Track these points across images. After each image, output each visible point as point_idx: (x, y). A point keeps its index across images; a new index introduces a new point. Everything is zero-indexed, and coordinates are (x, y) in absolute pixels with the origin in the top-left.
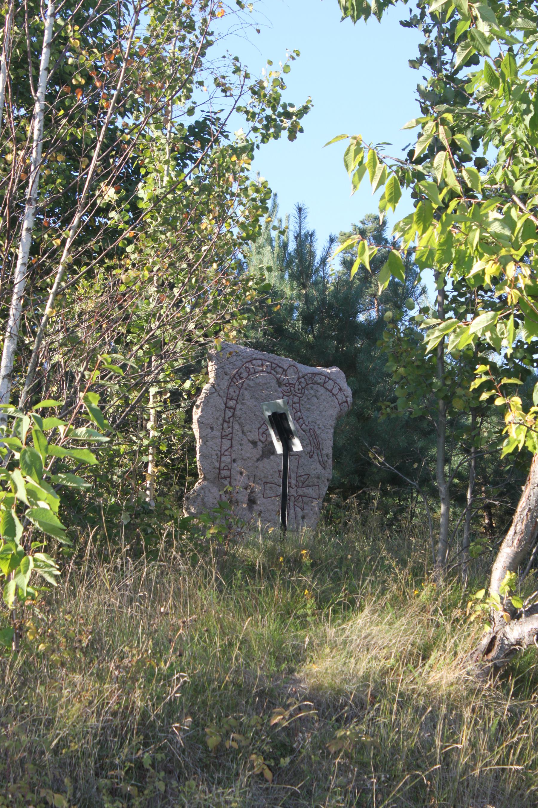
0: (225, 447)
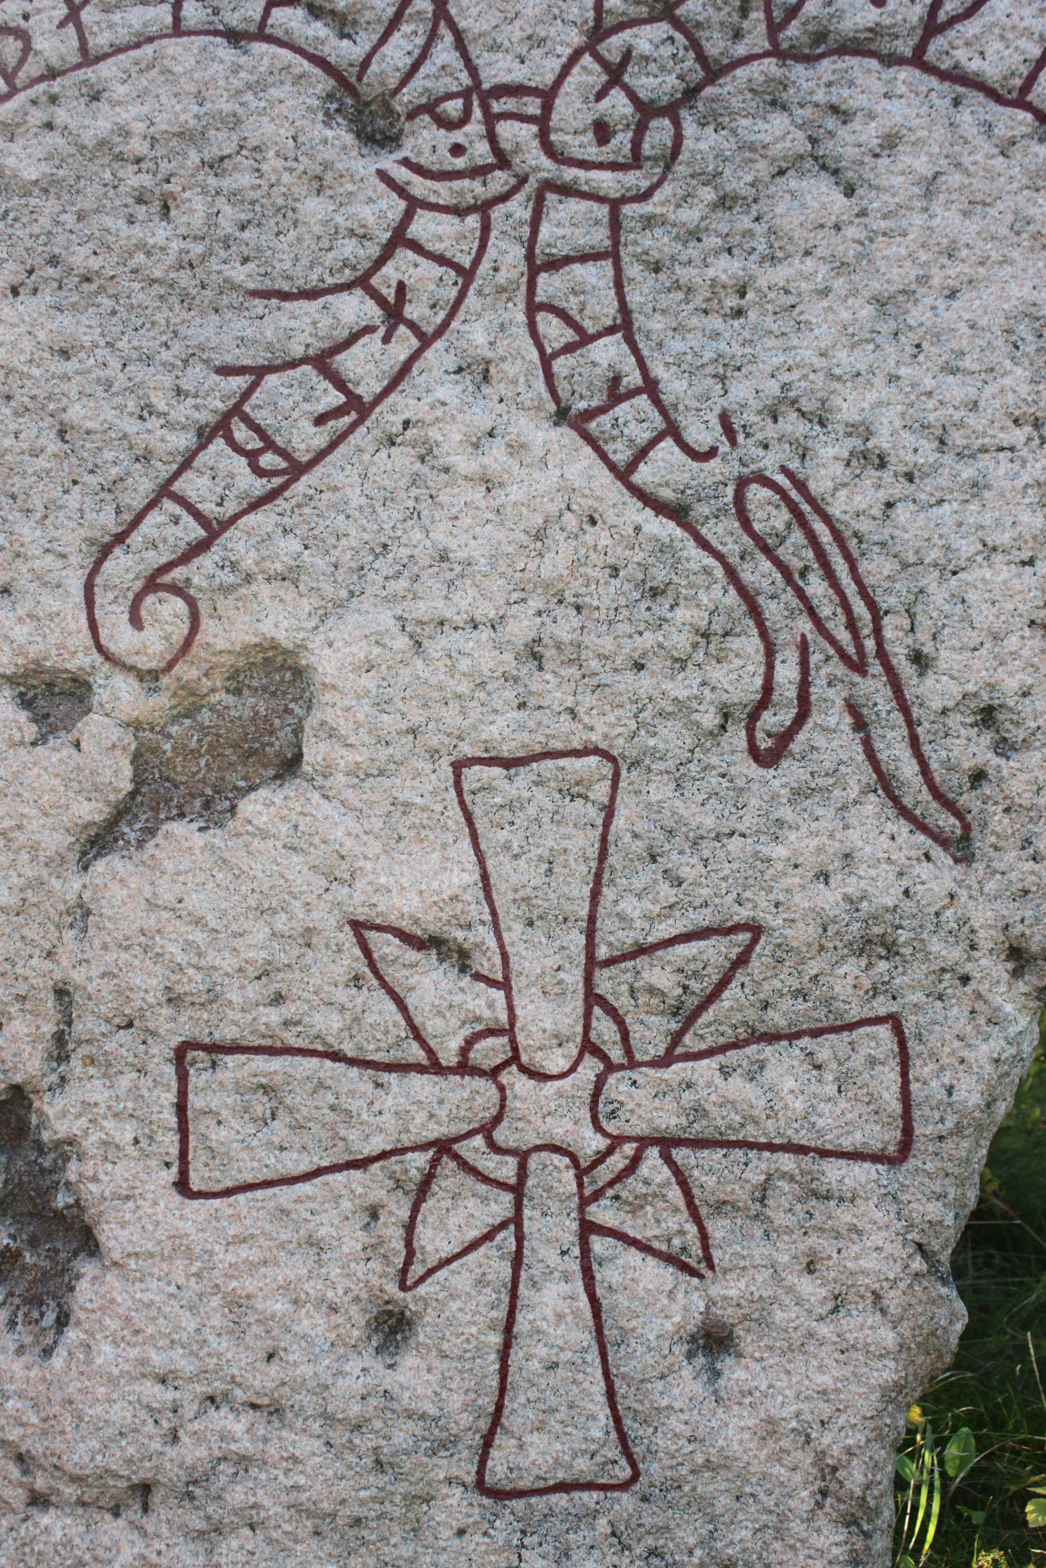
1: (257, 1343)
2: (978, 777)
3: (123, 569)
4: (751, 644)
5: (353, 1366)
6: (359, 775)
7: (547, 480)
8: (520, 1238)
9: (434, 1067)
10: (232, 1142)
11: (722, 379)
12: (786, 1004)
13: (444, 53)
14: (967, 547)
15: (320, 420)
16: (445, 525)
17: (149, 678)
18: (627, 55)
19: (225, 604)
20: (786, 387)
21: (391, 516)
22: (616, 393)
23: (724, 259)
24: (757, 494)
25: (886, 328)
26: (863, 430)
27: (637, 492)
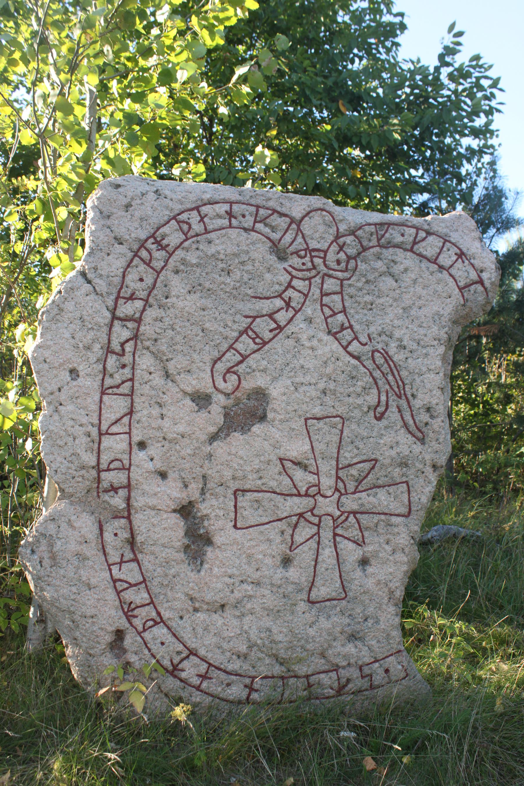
0: (109, 416)
1: (254, 565)
2: (427, 424)
3: (221, 367)
4: (375, 391)
5: (278, 571)
6: (282, 421)
7: (327, 349)
8: (319, 537)
9: (299, 495)
10: (249, 514)
11: (368, 326)
12: (382, 479)
13: (300, 239)
14: (424, 369)
15: (271, 331)
16: (302, 359)
17: (227, 395)
18: (344, 244)
19: (248, 377)
20: (383, 328)
21: (289, 356)
22: (343, 328)
23: (368, 296)
24: (377, 355)
25: (405, 315)
26: (400, 340)
27: (348, 353)
